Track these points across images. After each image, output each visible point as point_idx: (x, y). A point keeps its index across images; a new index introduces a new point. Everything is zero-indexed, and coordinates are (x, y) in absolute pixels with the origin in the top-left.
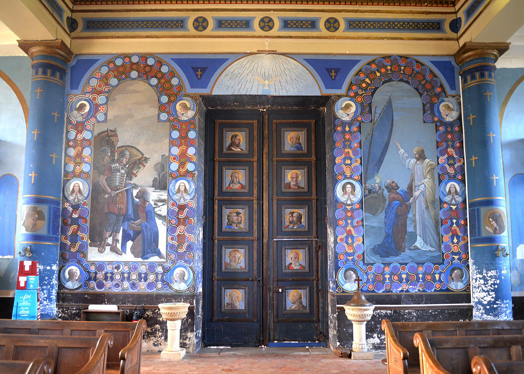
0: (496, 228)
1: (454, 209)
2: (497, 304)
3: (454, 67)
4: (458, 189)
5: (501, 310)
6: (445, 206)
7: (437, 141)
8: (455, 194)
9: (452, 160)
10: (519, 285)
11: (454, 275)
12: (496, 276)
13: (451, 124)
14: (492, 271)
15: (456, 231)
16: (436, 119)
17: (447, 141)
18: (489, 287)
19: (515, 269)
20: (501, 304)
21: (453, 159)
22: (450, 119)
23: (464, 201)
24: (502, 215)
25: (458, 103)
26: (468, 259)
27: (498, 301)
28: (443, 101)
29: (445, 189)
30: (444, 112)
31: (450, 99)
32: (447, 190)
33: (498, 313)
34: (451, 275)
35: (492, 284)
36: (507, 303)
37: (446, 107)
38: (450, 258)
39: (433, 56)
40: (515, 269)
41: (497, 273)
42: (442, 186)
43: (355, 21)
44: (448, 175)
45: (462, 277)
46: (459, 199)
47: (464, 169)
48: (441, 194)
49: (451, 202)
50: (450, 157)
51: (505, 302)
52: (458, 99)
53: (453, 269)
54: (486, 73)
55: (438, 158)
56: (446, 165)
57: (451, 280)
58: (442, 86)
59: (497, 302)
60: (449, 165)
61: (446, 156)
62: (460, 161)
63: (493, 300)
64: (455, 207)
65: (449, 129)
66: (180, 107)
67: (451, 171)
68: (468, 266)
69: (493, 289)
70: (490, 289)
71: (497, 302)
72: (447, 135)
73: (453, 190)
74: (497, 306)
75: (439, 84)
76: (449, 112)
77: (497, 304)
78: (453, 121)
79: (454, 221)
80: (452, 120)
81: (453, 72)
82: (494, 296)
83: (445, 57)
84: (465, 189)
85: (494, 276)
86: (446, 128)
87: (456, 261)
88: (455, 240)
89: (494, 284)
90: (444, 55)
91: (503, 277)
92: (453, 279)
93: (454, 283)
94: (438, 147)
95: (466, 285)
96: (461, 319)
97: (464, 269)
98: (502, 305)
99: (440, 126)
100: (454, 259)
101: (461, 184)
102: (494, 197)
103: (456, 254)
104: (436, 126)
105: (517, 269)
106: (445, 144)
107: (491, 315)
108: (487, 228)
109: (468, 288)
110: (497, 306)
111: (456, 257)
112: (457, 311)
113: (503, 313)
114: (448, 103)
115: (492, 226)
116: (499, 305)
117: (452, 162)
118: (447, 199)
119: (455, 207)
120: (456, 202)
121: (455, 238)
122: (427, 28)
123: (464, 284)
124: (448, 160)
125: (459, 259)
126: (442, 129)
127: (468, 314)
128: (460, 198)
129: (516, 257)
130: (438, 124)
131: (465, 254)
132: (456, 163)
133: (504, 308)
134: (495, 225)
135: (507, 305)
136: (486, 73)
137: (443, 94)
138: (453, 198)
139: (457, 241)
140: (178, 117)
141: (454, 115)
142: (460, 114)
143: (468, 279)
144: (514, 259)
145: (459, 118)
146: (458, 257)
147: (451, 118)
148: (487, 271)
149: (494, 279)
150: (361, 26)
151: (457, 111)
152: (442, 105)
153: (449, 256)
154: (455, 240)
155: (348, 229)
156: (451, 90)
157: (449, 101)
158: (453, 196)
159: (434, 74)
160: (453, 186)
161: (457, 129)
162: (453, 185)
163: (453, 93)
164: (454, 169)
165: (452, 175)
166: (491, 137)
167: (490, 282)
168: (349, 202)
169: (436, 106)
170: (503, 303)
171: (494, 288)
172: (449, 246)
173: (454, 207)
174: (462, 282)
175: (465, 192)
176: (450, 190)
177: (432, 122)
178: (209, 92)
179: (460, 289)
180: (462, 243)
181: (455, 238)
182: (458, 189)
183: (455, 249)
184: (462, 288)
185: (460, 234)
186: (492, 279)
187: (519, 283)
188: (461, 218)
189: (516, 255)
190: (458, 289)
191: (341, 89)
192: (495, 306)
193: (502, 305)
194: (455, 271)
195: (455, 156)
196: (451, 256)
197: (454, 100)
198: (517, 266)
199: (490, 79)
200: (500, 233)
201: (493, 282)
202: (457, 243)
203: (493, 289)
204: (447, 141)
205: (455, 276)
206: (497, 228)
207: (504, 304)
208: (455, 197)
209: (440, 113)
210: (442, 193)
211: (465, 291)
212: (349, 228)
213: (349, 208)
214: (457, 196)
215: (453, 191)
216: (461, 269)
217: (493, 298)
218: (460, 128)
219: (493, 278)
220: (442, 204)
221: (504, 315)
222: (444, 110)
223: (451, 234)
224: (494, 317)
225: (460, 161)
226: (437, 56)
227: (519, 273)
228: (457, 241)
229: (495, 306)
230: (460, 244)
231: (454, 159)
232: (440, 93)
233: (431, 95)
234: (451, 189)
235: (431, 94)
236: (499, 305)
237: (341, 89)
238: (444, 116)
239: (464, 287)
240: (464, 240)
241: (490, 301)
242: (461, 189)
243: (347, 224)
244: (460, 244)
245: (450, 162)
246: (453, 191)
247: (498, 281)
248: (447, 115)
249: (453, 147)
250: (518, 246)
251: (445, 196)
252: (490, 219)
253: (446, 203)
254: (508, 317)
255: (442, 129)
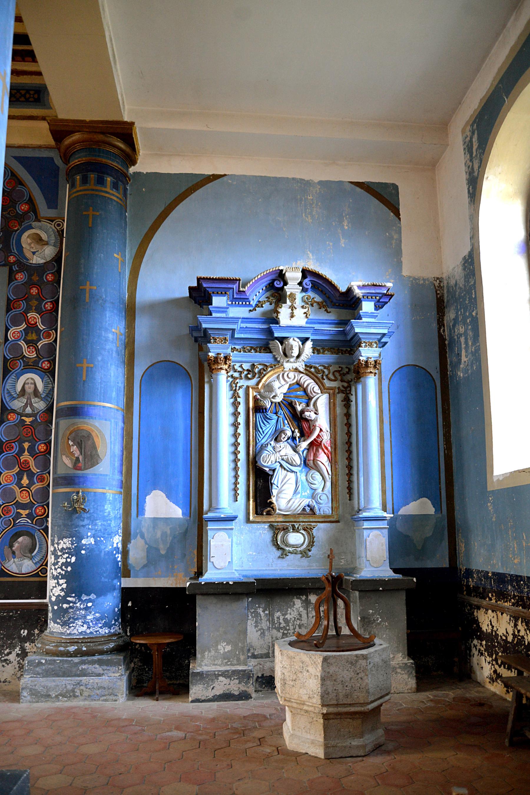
0: (77, 459)
1: (28, 423)
2: (69, 602)
3: (58, 168)
4: (40, 386)
5: (74, 613)
6: (12, 417)
7: (8, 298)
8: (32, 396)
9: (34, 335)
10: (145, 566)
11: (16, 545)
12: (69, 549)
13: (41, 269)
14: (65, 540)
15: (28, 463)
16: (12, 259)
17: (27, 298)
18: (59, 570)
19: (139, 536)
20: (75, 603)
21: (36, 332)
22: (39, 259)
23: (50, 409)
24: (93, 434)
25: (58, 231)
26: (48, 516)
27: (71, 597)
28: (30, 227)
29: (14, 387)
30: (28, 248)
31: (45, 224)
32: (19, 388)
33: (69, 619)
34: (11, 546)
35: (63, 564)
36: (90, 601)
37: (34, 239)
38: (13, 513)
39: (19, 147)
40: (139, 536)
41: (72, 544)
42: (9, 381)
43: (20, 90)
44: (24, 361)
45: (32, 550)
46: (40, 405)
47: (56, 350)
48: (6, 396)
49: (24, 410)
50: (32, 328)
51: (84, 597)
52: (59, 225)
53: (17, 535)
54: (92, 176)
55: (7, 330)
56: (22, 343)
57: (11, 555)
58: (31, 202)
59: (69, 599)
60: (27, 342)
61: (24, 326)
62: (49, 336)
63: (62, 594)
64: (31, 419)
65: (35, 278)
66: (29, 241)
67: (30, 354)
68: (46, 530)
69: (63, 573)
70: (60, 573)
71: (69, 599)
72: (31, 289)
73: (30, 388)
74: (68, 606)
75: (26, 198)
76: (38, 246)
77: (69, 602)
78: (45, 263)
79: (26, 445)
80: (42, 261)
81: (57, 176)
82: (64, 586)
83: (42, 150)
84: (53, 388)
85: (67, 548)
86: (30, 276)
87: (24, 520)
88: (25, 481)
89: (66, 564)
90: (40, 147)
91: (83, 552)
92: (14, 553)
93: (16, 560)
94: (8, 310)
95: (39, 565)
96: (24, 629)
97: (37, 535)
98: (78, 605)
99: (18, 272)
100: (19, 515)
101: (46, 378)
102: (88, 400)
103: (24, 506)
104: (11, 272)
105: (143, 537)
106: (23, 305)
107: (58, 623)
108: (64, 457)
109: (43, 571)
110: (68, 606)
111: (24, 512)
112: (16, 613)
113: (77, 619)
114: (38, 232)
115: (72, 454)
116: (71, 604)
117: (33, 336)
118: (17, 404)
119: (31, 419)
120: (33, 411)
121: (25, 478)
122: (15, 99)
123: (36, 564)
124: (26, 334)
125: (29, 516)
126: (21, 277)
127: (39, 618)
128: (42, 402)
129: (144, 514)
130: (15, 268)
131: (43, 506)
132: (41, 340)
133: (81, 609)
134: (77, 453)
135: (90, 604)
136: (109, 179)
137: (32, 214)
138: (29, 403)
139: (27, 482)
140: (28, 260)
141: (49, 252)
142: (60, 251)
143: (44, 551)
144: (140, 518)
145: (58, 259)
146: (27, 512)
147: (42, 258)
148: (58, 540)
149: (67, 555)
150: (30, 97)
151: (54, 246)
152: (26, 234)
153: (10, 511)
154: (25, 481)
155: (22, 458)
156: (49, 208)
157: (40, 228)
158: (29, 399)
159: (18, 179)
160: (30, 381)
161: (50, 278)
162: (32, 379)
163: (51, 213)
164: (37, 350)
165: (32, 360)
166: (87, 290)
167: (61, 561)
168: (28, 410)
169: (15, 236)
170: (80, 600)
171: (66, 572)
172: (12, 491)
173: (28, 420)
174: (31, 558)
175: (53, 392)
176: (23, 389)
177: (4, 265)
178: (42, 216)
179: (27, 572)
180: (37, 486)
181: (25, 478)
182: (40, 386)
183: (23, 498)
184: (30, 570)
185: (35, 470)
186: (64, 554)
187: (145, 562)
188: (40, 440)
189: (143, 509)
190: (23, 572)
191: (49, 208)
192: (65, 606)
193: (78, 605)
194: (20, 539)
195: (41, 327)
196: (14, 510)
197: (51, 227)
198: (144, 530)
199: (99, 187)
200: (85, 469)
201: (64, 561)
202: (29, 486)
203: (63, 573)
204: (27, 298)
205: (20, 548)
206: (81, 458)
207: (83, 602)
208: (33, 400)
209: (20, 248)
210: (9, 392)
211: (37, 575)
212: (26, 456)
213: (28, 420)
214: (37, 399)
215: (29, 389)
216: (32, 536)
217: (62, 590)
218: (57, 276)
219: (67, 553)
220: (6, 414)
221: (80, 622)
222: (30, 244)
223: (17, 469)
224: (62, 626)
225: (49, 336)
226: (28, 147)
227: (146, 543)
228: (27, 482)
229: (65, 606)
230: (34, 488)
231: (38, 331)
232: (26, 213)
233: (8, 216)
234: (26, 386)
235: (9, 214)
236: (71, 604)
237: (49, 208)
238: (28, 254)
239: (35, 568)
240: (41, 479)
241: (59, 595)
242: (45, 387)
243: (22, 451)
244: (34, 488)
245: (29, 338)
246: (29, 389)
247: (73, 559)
248: (34, 253)
249: (39, 311)
250: (149, 494)
251: (14, 398)
252: (71, 443)
253: (13, 411)
254: (89, 628)
255: (21, 277)
